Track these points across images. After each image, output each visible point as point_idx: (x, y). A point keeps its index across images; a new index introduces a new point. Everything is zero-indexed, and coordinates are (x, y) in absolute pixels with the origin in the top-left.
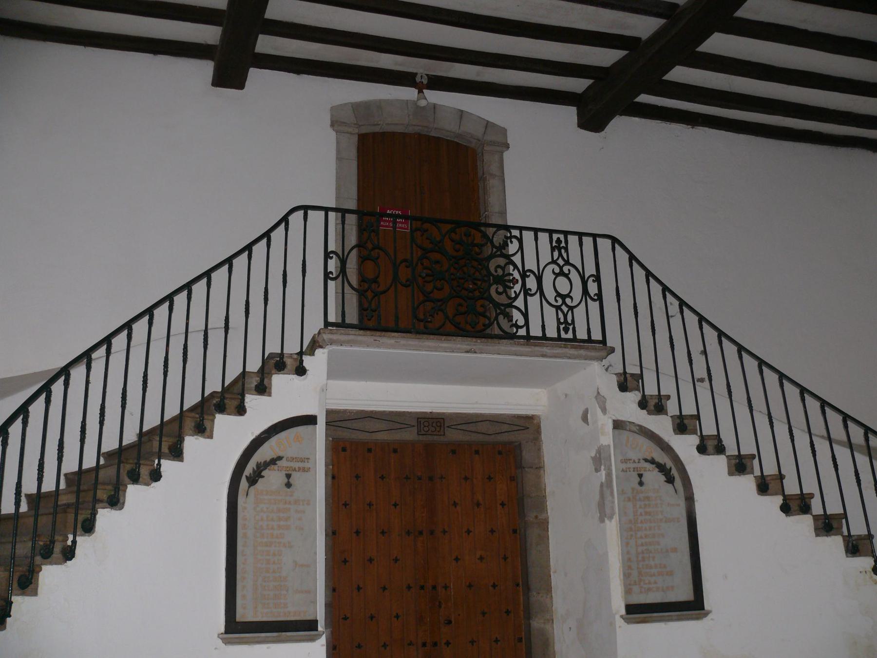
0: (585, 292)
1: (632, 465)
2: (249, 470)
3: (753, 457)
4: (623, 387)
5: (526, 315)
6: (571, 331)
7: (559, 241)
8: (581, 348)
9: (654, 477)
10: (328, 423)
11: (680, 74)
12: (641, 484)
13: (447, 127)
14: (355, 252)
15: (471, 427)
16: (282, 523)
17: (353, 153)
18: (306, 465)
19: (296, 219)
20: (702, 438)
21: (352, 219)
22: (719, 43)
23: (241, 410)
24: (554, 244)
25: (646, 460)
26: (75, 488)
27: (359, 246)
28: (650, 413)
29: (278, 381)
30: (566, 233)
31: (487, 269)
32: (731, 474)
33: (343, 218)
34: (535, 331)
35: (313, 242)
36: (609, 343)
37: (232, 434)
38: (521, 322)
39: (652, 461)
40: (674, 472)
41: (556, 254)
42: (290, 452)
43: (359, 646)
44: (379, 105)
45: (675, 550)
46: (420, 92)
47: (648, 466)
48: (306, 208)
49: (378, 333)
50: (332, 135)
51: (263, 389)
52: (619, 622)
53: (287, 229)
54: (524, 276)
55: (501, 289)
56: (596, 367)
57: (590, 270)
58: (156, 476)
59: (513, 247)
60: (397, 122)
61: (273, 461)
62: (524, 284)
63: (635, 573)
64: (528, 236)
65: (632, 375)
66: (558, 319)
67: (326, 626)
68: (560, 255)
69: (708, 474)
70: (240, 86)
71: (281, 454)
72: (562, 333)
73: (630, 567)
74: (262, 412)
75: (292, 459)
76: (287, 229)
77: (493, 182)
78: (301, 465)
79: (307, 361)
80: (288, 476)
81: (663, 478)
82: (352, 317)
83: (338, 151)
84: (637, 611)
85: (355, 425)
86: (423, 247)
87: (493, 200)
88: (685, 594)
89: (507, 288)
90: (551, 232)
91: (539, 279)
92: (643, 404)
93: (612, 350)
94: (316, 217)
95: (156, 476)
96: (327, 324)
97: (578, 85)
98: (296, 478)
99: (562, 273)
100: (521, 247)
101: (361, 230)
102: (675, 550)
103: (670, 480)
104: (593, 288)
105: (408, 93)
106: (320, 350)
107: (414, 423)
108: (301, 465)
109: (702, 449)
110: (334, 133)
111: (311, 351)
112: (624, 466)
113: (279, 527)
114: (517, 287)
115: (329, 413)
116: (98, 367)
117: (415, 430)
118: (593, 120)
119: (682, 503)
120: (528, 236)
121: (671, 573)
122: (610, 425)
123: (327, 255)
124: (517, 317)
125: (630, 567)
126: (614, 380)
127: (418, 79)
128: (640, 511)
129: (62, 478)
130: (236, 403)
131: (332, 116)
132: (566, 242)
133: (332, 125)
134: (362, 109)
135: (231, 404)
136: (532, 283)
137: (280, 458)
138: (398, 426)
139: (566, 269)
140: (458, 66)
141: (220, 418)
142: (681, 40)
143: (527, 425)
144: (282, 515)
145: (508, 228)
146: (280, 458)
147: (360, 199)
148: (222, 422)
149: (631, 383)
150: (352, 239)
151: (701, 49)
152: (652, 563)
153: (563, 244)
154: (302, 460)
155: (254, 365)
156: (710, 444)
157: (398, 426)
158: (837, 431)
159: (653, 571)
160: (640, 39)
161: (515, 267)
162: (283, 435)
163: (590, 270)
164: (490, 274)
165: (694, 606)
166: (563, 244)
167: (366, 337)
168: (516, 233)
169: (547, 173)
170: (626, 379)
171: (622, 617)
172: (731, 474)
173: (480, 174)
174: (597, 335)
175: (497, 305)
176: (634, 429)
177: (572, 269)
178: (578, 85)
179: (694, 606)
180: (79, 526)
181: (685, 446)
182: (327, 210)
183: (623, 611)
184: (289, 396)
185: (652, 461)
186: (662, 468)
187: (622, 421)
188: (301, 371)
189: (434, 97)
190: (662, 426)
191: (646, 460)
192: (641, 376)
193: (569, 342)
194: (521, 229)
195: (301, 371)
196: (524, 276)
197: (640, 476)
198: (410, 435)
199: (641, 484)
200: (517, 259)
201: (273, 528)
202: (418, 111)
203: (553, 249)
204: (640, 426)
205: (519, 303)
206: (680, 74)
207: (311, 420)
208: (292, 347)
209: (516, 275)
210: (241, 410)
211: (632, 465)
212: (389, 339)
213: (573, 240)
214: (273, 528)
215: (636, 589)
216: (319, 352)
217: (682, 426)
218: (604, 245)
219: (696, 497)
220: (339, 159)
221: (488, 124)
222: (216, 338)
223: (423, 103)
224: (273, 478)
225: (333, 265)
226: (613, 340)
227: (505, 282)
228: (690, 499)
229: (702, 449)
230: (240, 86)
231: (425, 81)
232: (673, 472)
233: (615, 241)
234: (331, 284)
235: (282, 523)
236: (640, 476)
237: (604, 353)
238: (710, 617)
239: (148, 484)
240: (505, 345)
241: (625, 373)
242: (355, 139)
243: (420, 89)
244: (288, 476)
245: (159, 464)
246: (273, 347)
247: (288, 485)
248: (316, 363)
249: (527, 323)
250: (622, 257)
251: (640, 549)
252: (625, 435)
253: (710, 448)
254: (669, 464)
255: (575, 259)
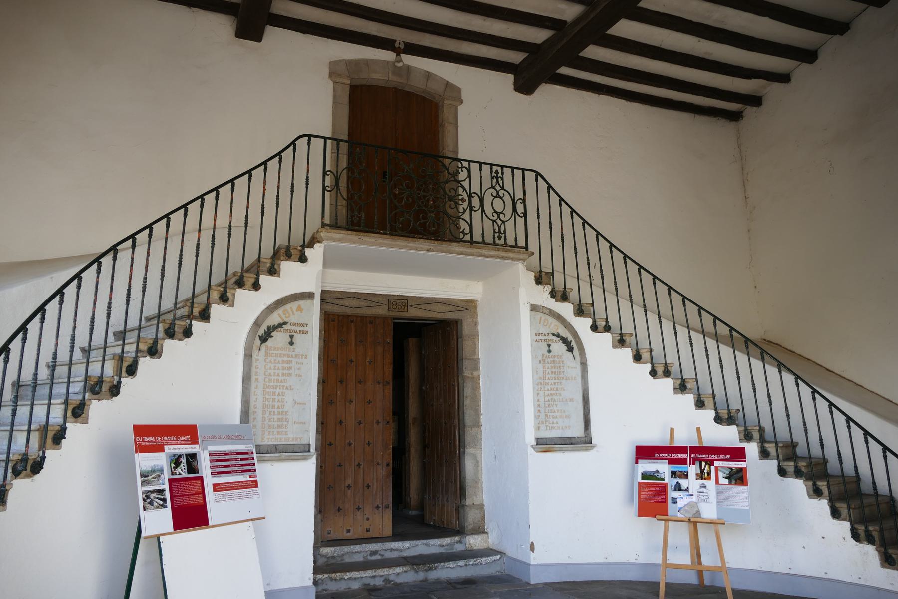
0: (515, 210)
1: (543, 338)
2: (261, 332)
3: (631, 335)
4: (539, 281)
5: (471, 226)
6: (503, 238)
7: (497, 172)
8: (510, 251)
9: (559, 348)
10: (322, 301)
11: (594, 52)
12: (549, 351)
13: (417, 84)
14: (345, 171)
15: (427, 307)
16: (285, 372)
17: (345, 100)
18: (305, 329)
19: (302, 144)
20: (594, 321)
21: (344, 147)
22: (625, 28)
23: (256, 286)
24: (494, 174)
25: (554, 335)
26: (121, 342)
27: (350, 169)
28: (557, 301)
29: (286, 266)
30: (502, 167)
31: (444, 189)
32: (614, 347)
33: (338, 145)
34: (477, 237)
35: (315, 162)
36: (530, 249)
37: (249, 305)
38: (467, 230)
39: (558, 336)
40: (573, 344)
41: (495, 180)
42: (293, 319)
43: (340, 465)
44: (367, 63)
45: (572, 400)
46: (398, 55)
47: (555, 338)
48: (309, 136)
49: (362, 234)
50: (330, 85)
51: (273, 271)
52: (531, 451)
53: (294, 151)
54: (470, 197)
55: (453, 206)
56: (520, 266)
57: (519, 195)
58: (187, 333)
59: (463, 175)
60: (378, 77)
61: (280, 326)
62: (470, 203)
63: (543, 415)
64: (475, 167)
65: (546, 273)
66: (494, 230)
67: (316, 450)
68: (497, 182)
69: (597, 345)
70: (259, 39)
71: (286, 320)
72: (497, 239)
73: (539, 411)
74: (273, 288)
75: (295, 324)
76: (294, 151)
77: (449, 128)
78: (301, 329)
79: (308, 252)
80: (291, 337)
81: (566, 348)
82: (342, 220)
83: (335, 96)
84: (544, 444)
85: (341, 302)
86: (394, 172)
87: (449, 141)
88: (577, 431)
89: (457, 204)
90: (491, 165)
91: (515, 210)
92: (553, 294)
93: (533, 253)
94: (317, 144)
95: (187, 333)
96: (324, 225)
97: (516, 57)
98: (298, 338)
99: (498, 196)
100: (469, 176)
101: (350, 154)
102: (572, 400)
103: (570, 349)
104: (520, 208)
105: (387, 56)
106: (318, 244)
107: (386, 303)
108: (301, 329)
109: (594, 328)
110: (331, 83)
111: (311, 245)
112: (538, 338)
113: (283, 375)
114: (466, 204)
115: (323, 292)
116: (141, 251)
117: (386, 307)
118: (525, 86)
119: (579, 367)
120: (475, 167)
121: (569, 417)
122: (529, 308)
123: (325, 173)
124: (464, 225)
125: (539, 411)
126: (532, 275)
127: (397, 45)
128: (548, 371)
129: (143, 319)
130: (252, 280)
131: (330, 69)
132: (503, 173)
133: (330, 76)
134: (354, 65)
135: (249, 279)
136: (476, 202)
137: (285, 323)
138: (374, 304)
139: (501, 193)
140: (427, 36)
141: (240, 292)
142: (594, 29)
143: (469, 306)
144: (286, 365)
145: (460, 160)
146: (285, 323)
147: (350, 135)
148: (242, 295)
149: (544, 278)
150: (344, 163)
151: (609, 32)
152: (555, 409)
153: (500, 175)
154: (302, 325)
155: (268, 251)
156: (660, 370)
157: (374, 304)
158: (694, 320)
159: (555, 414)
160: (565, 22)
161: (465, 189)
162: (288, 307)
163: (519, 195)
164: (446, 193)
165: (586, 442)
166: (500, 175)
167: (353, 236)
168: (466, 164)
169: (492, 122)
170: (541, 276)
171: (532, 446)
172: (614, 347)
173: (440, 121)
174: (521, 242)
175: (449, 217)
176: (545, 311)
177: (506, 193)
178: (516, 57)
179: (586, 442)
180: (124, 370)
181: (582, 325)
182: (325, 139)
183: (534, 443)
184: (297, 277)
185: (558, 336)
186: (564, 341)
187: (538, 306)
188: (303, 259)
189: (410, 60)
190: (566, 310)
191: (554, 335)
192: (552, 274)
193: (500, 244)
194: (470, 162)
195: (303, 259)
196: (470, 197)
197: (549, 346)
198: (382, 311)
199: (549, 351)
200: (466, 184)
201: (278, 375)
202: (397, 71)
203: (492, 178)
204: (550, 310)
205: (467, 216)
206: (594, 52)
207: (310, 296)
208: (297, 239)
209: (466, 197)
210: (256, 286)
211: (543, 338)
212: (370, 238)
213: (508, 172)
214: (278, 375)
215: (543, 427)
216: (317, 245)
217: (580, 312)
218: (530, 176)
219: (588, 363)
220: (335, 103)
221: (448, 84)
222: (238, 234)
223: (400, 65)
224: (279, 338)
225: (329, 181)
226: (533, 246)
227: (455, 200)
228: (584, 365)
229: (594, 328)
230: (259, 39)
231: (402, 47)
232: (571, 344)
233: (538, 174)
234: (327, 194)
235: (285, 372)
236: (549, 346)
237: (525, 256)
238: (595, 449)
239: (181, 340)
240: (455, 246)
241: (541, 271)
242: (348, 89)
243: (398, 52)
244: (291, 337)
245: (190, 325)
246: (282, 241)
247: (291, 344)
248: (315, 253)
249: (471, 231)
250: (542, 185)
251: (547, 399)
252: (539, 315)
253: (600, 328)
254: (570, 338)
255: (508, 186)
